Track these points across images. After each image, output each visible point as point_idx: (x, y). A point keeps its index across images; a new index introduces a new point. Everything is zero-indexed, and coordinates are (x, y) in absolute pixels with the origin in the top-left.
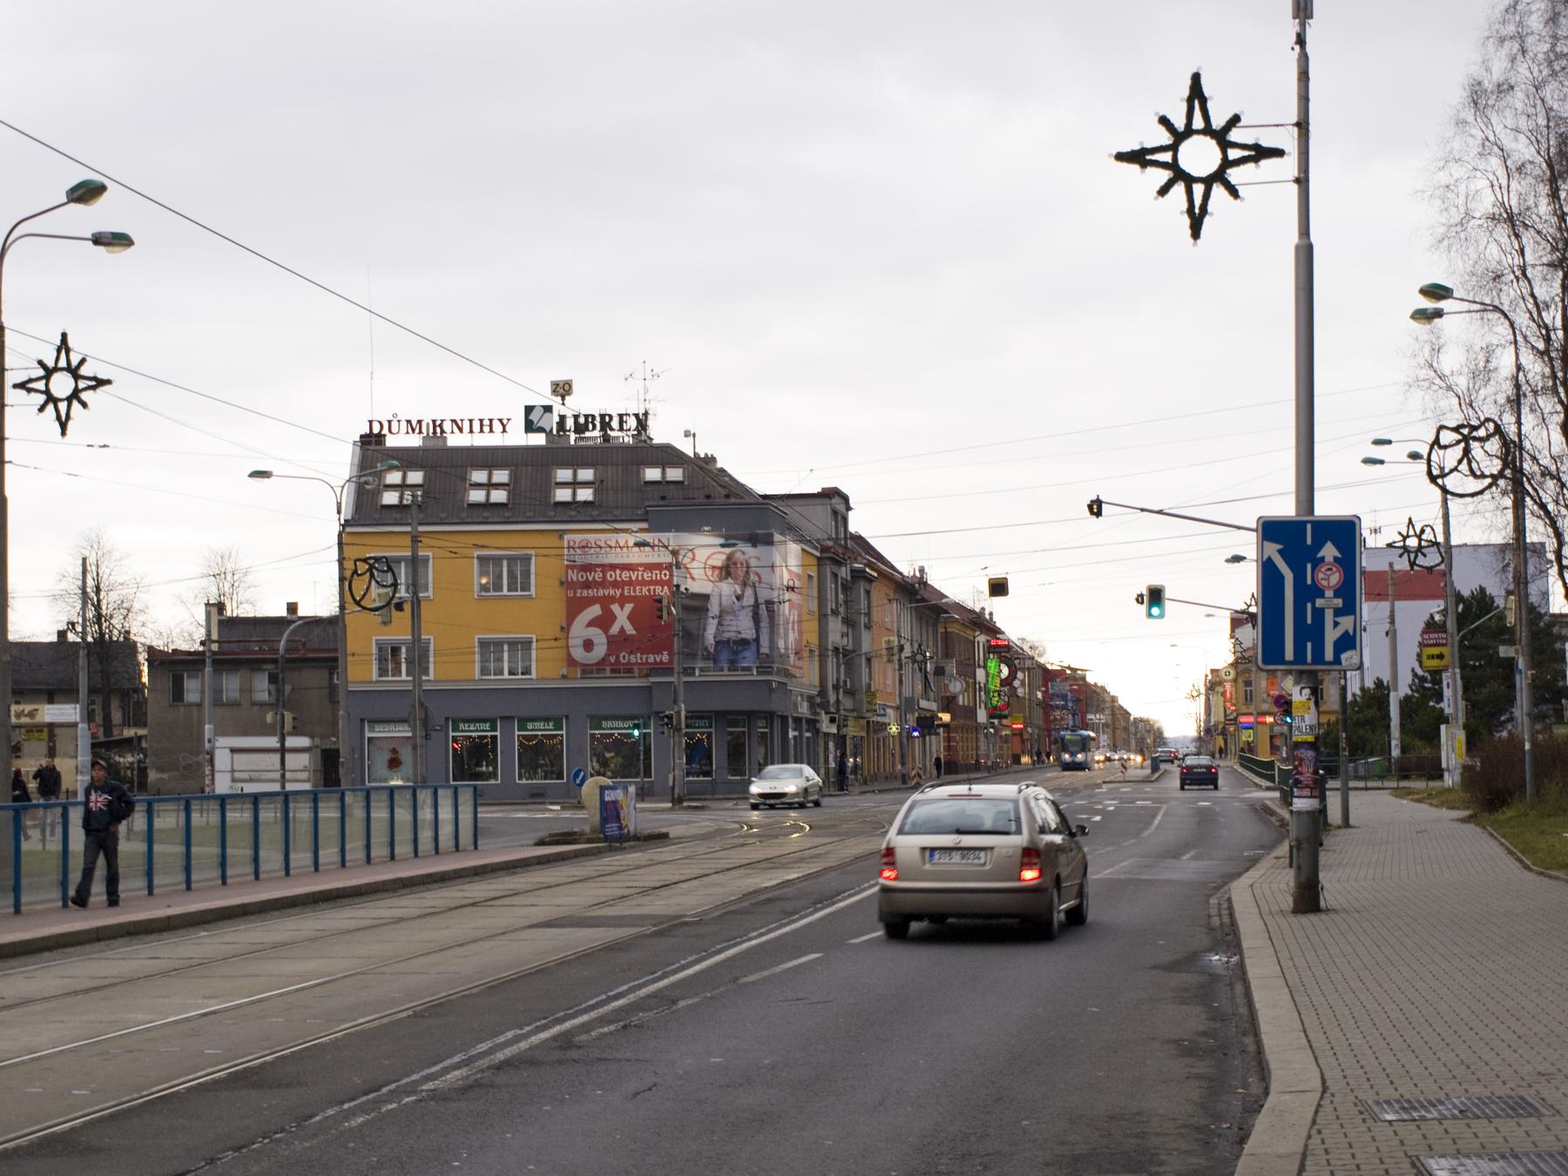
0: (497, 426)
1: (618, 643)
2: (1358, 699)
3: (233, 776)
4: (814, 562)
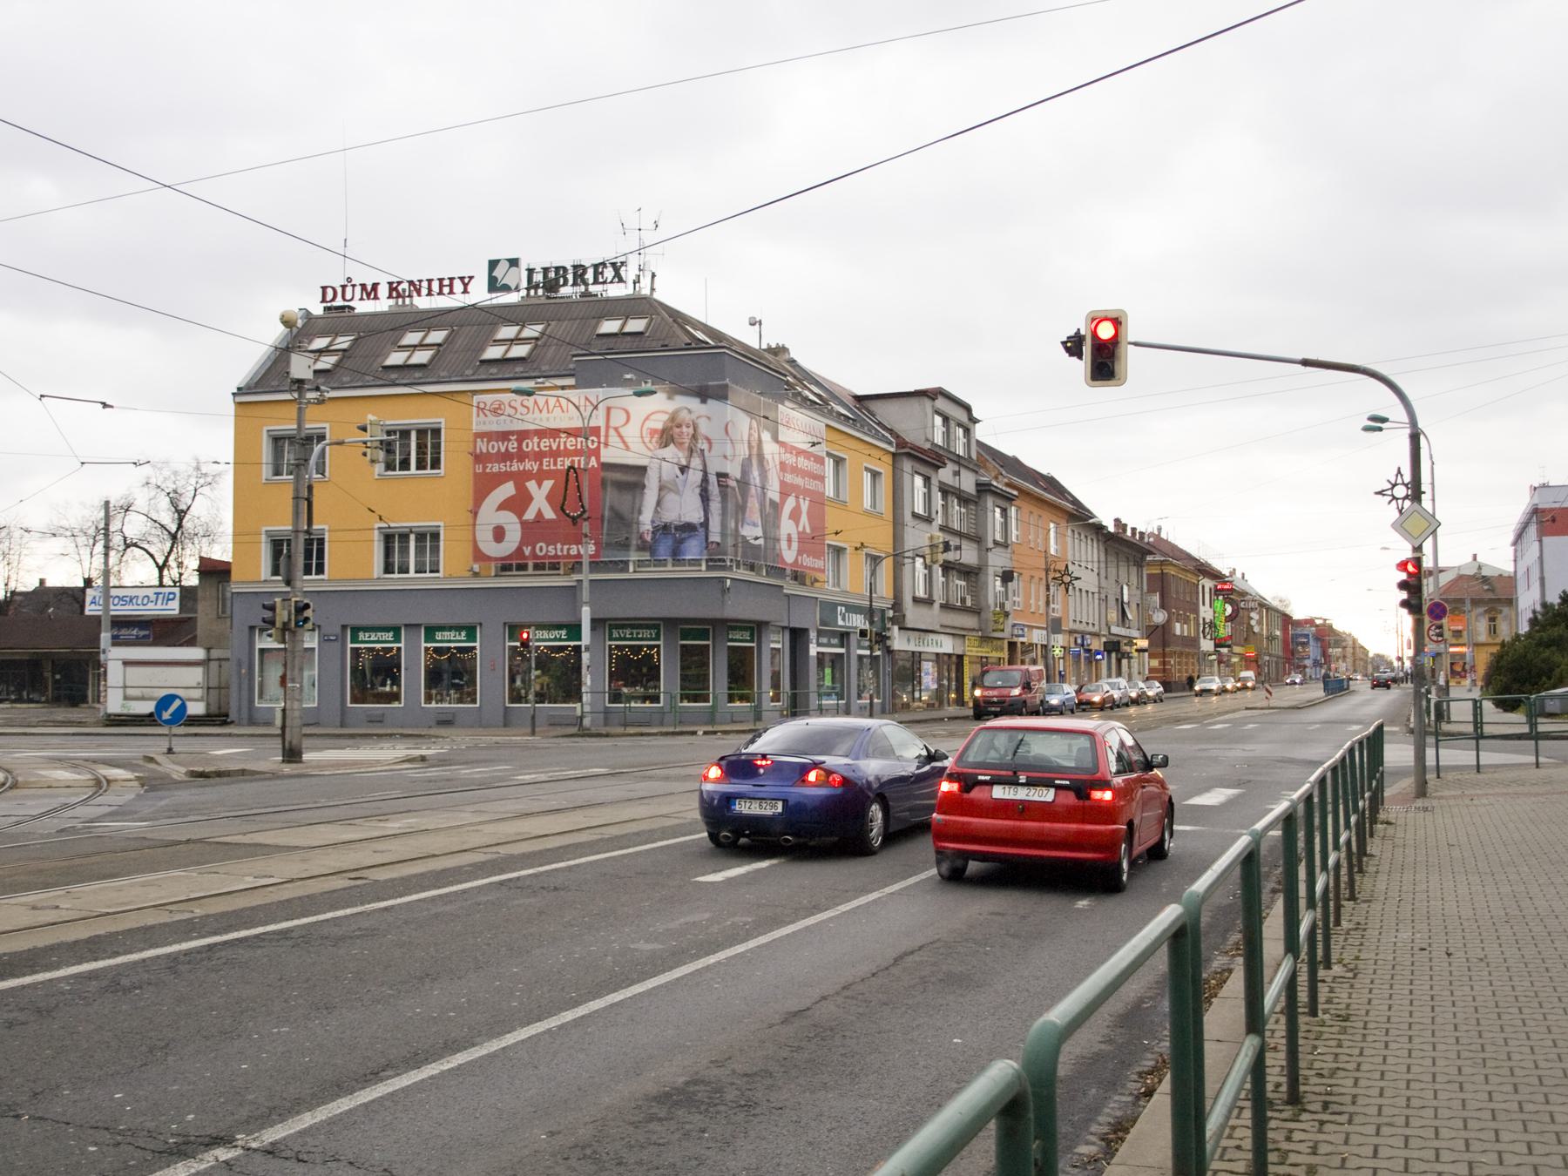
0: (458, 286)
1: (534, 530)
2: (1539, 617)
3: (125, 693)
4: (889, 459)
